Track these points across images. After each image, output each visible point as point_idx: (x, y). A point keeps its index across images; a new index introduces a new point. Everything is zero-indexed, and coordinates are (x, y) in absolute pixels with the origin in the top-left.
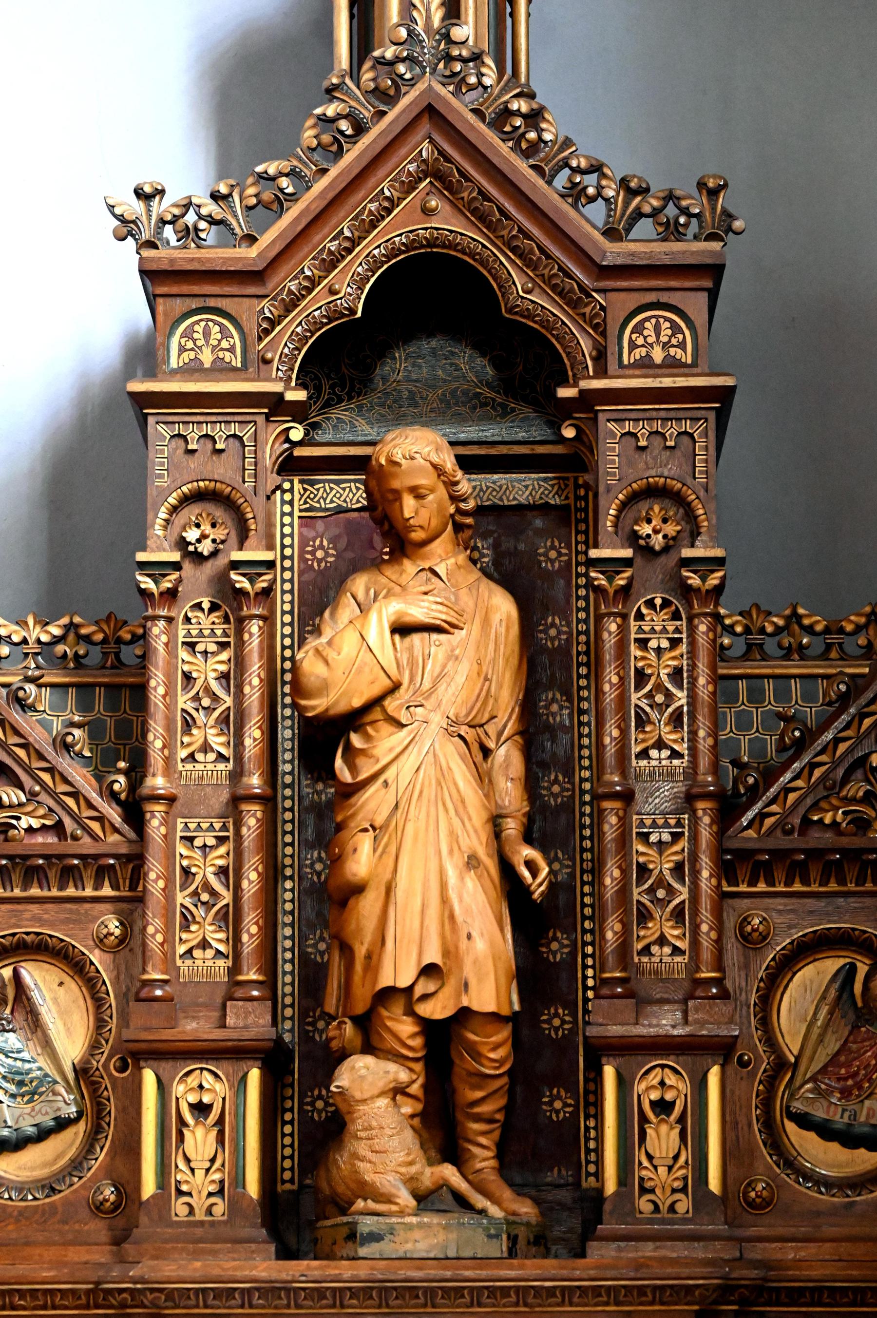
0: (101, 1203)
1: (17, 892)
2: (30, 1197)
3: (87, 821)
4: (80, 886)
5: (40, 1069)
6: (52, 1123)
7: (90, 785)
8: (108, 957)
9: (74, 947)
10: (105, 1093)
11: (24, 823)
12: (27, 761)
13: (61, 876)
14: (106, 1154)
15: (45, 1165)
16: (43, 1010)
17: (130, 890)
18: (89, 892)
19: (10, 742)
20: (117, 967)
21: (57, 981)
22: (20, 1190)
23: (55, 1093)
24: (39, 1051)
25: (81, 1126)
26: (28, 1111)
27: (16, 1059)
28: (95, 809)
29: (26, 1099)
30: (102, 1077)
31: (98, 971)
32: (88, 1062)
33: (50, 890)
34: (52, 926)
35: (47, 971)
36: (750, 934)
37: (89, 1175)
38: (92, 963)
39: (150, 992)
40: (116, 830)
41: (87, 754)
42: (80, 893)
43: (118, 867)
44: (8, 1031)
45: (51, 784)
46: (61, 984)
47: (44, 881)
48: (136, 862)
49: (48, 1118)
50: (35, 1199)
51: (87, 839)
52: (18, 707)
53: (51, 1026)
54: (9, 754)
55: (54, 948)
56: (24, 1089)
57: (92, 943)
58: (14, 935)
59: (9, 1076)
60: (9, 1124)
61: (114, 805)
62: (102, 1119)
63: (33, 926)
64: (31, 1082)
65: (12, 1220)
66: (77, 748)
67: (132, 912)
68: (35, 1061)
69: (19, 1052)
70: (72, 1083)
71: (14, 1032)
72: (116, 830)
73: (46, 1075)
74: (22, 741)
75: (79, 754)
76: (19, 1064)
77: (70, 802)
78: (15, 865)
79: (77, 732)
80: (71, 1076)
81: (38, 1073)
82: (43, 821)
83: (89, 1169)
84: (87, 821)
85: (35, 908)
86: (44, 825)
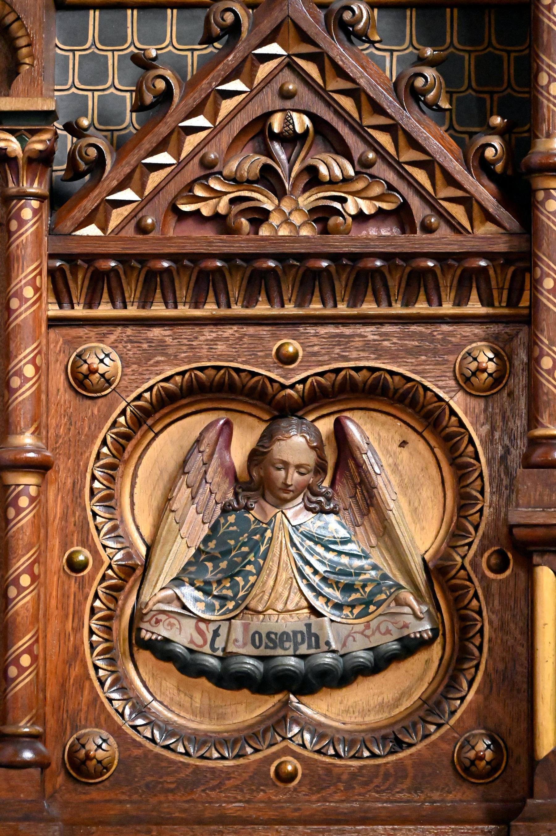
0: (473, 762)
1: (343, 309)
2: (366, 754)
3: (445, 204)
4: (435, 299)
5: (375, 567)
6: (395, 646)
7: (451, 152)
8: (478, 405)
9: (426, 389)
10: (475, 603)
11: (351, 208)
12: (356, 116)
13: (408, 285)
14: (477, 692)
15: (382, 707)
16: (380, 482)
17: (508, 306)
18: (448, 309)
19: (330, 88)
20: (490, 419)
21: (398, 439)
22: (351, 744)
23: (399, 603)
24: (373, 541)
25: (436, 649)
26: (361, 628)
27: (340, 553)
28: (458, 185)
29: (356, 611)
30: (470, 580)
31: (461, 424)
32: (447, 557)
33: (283, 306)
34: (394, 357)
35: (384, 424)
36: (86, 377)
37: (452, 721)
38: (453, 413)
39: (547, 454)
40: (489, 217)
41: (445, 105)
42: (434, 310)
43: (491, 272)
44: (328, 513)
45: (391, 149)
46: (403, 444)
47: (275, 294)
48: (521, 265)
49: (388, 638)
50: (374, 756)
51: (444, 231)
52: (342, 36)
53: (392, 505)
54: (329, 105)
55: (396, 390)
56: (354, 596)
57: (452, 383)
58: (337, 371)
59: (332, 576)
60: (334, 647)
61: (486, 182)
62: (469, 639)
63: (367, 359)
64: (364, 586)
65: (341, 786)
66: (431, 96)
67: (511, 338)
68: (366, 557)
69: (345, 542)
70: (423, 588)
71: (336, 513)
72: (489, 217)
73: (385, 577)
74: (348, 85)
75: (434, 107)
76: (345, 560)
77: (421, 176)
78: (287, 269)
79: (430, 73)
80: (420, 577)
81: (373, 573)
82: (378, 204)
83: (453, 713)
84: (445, 204)
85: (369, 332)
86: (380, 211)
